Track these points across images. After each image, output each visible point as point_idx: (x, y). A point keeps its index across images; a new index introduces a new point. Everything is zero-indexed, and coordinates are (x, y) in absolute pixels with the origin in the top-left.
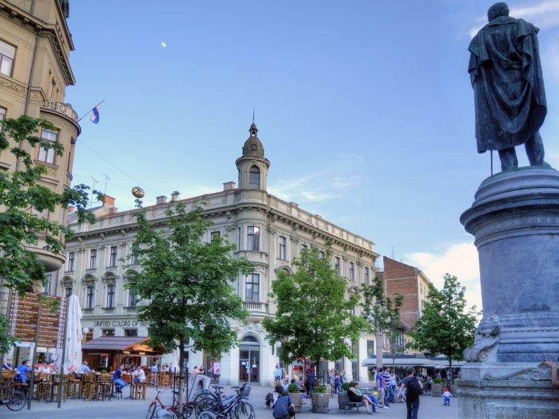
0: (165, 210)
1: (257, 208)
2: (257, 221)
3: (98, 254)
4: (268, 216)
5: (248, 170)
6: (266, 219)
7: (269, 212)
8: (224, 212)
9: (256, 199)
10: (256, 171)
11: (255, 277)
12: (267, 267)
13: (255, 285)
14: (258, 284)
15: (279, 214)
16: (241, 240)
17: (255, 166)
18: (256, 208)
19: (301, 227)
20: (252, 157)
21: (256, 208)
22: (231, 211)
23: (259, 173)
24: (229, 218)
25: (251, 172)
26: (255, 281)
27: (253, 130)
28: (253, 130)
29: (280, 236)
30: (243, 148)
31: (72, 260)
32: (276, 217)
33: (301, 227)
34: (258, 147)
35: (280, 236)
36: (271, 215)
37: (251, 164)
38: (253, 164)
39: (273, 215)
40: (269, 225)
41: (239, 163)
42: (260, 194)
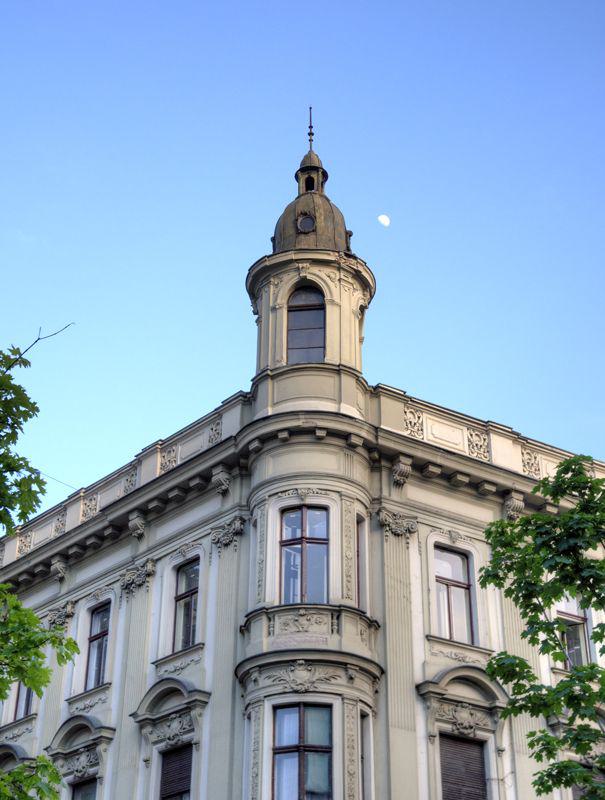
0: (47, 502)
1: (311, 431)
2: (314, 484)
3: (118, 620)
4: (374, 466)
5: (282, 300)
6: (359, 471)
7: (369, 447)
8: (206, 477)
9: (310, 396)
10: (309, 300)
11: (314, 718)
12: (376, 674)
13: (312, 757)
14: (327, 751)
15: (420, 453)
16: (352, 554)
17: (306, 287)
18: (304, 433)
19: (421, 469)
20: (300, 267)
21: (304, 433)
22: (228, 465)
23: (322, 307)
24: (225, 493)
25: (291, 310)
26: (314, 737)
27: (311, 175)
28: (311, 175)
29: (439, 547)
30: (273, 239)
31: (99, 639)
32: (405, 466)
33: (421, 469)
34: (321, 222)
35: (439, 547)
36: (381, 457)
37: (289, 280)
38: (295, 279)
39: (393, 457)
40: (378, 500)
41: (258, 280)
42: (328, 381)
